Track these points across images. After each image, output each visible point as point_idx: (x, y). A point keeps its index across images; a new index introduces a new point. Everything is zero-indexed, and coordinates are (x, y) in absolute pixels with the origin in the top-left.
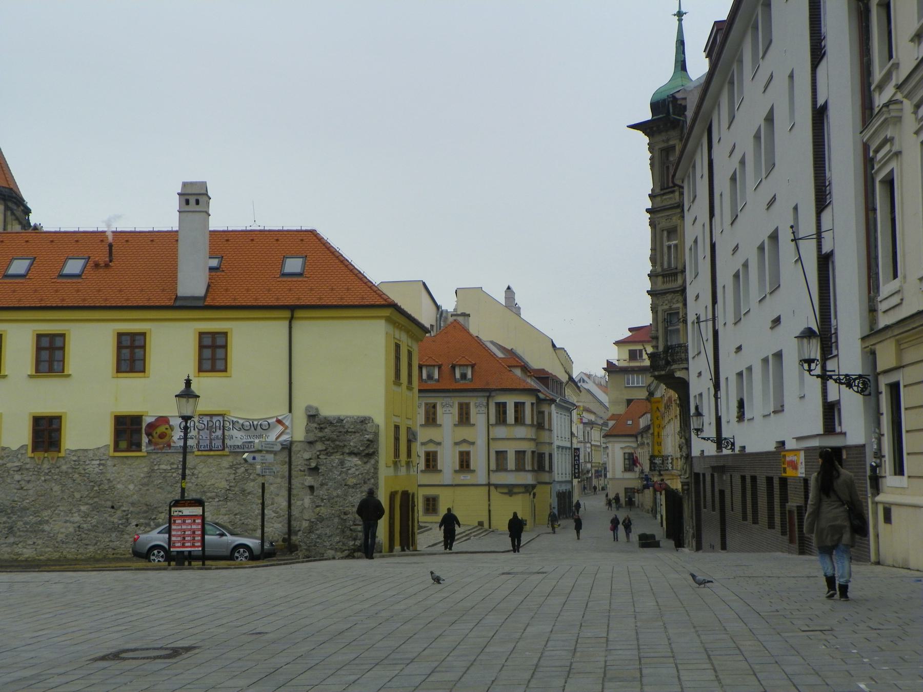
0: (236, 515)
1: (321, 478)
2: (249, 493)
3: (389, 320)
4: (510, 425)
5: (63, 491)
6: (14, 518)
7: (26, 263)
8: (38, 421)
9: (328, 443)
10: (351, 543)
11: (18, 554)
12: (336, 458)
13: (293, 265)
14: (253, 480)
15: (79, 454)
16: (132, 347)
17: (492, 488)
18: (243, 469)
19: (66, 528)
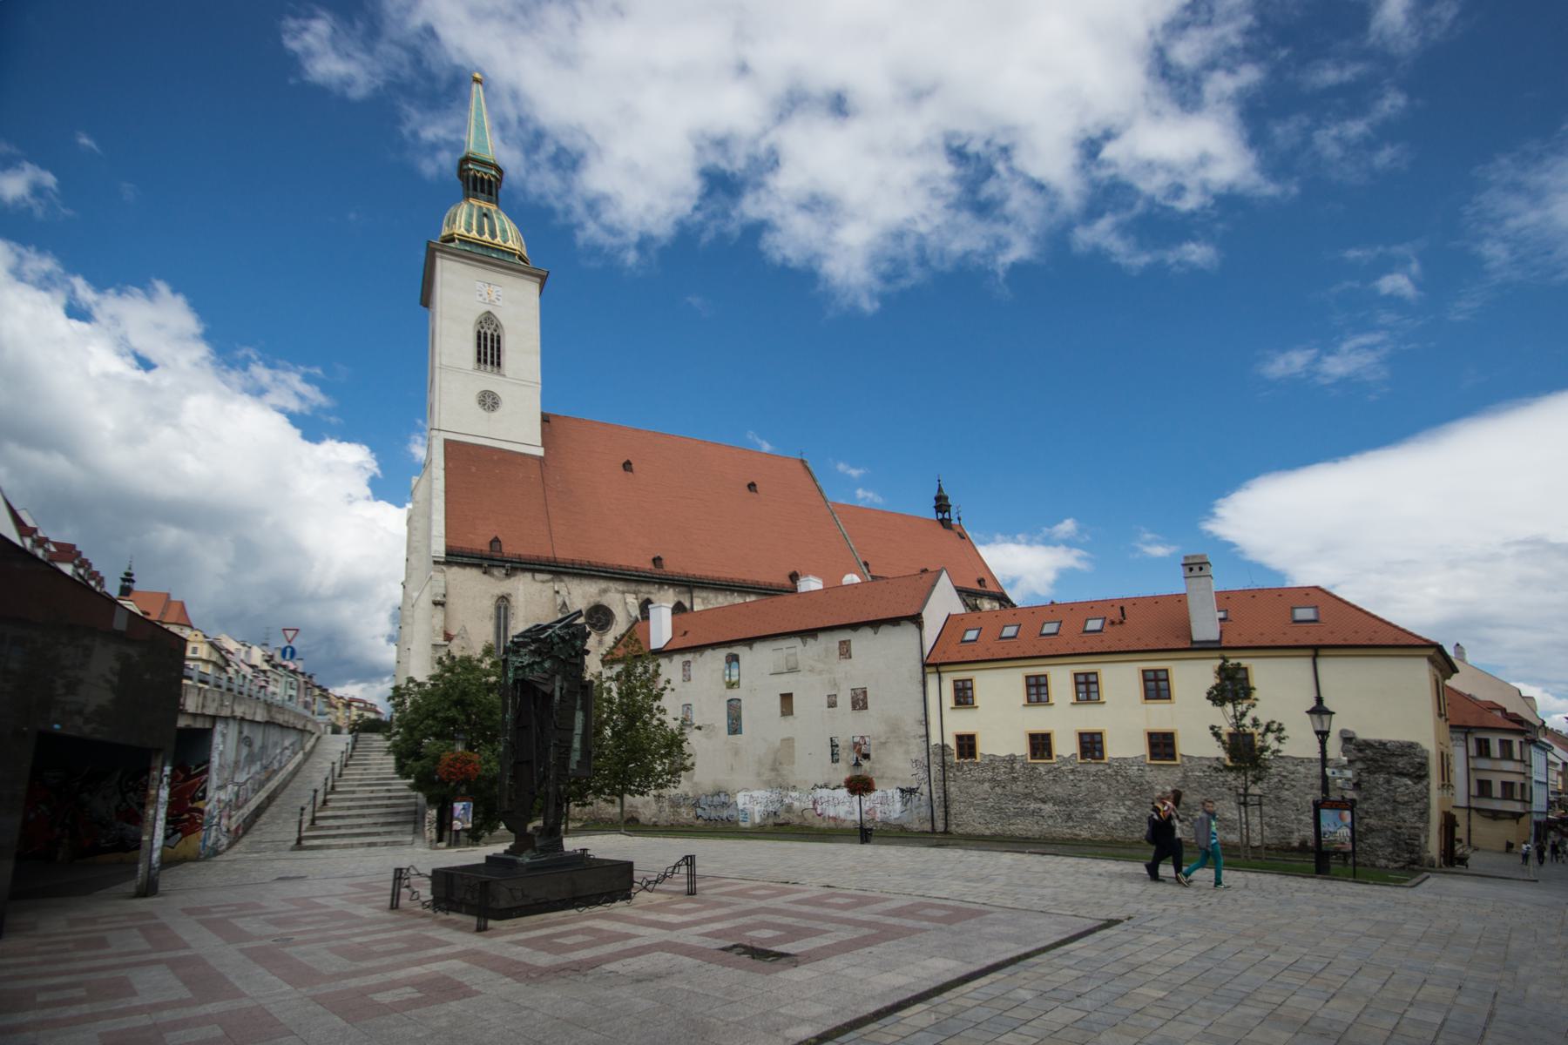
0: (1272, 817)
1: (1365, 793)
2: (1285, 801)
3: (1431, 660)
4: (1496, 759)
5: (1109, 789)
6: (1072, 807)
7: (976, 632)
8: (1152, 736)
9: (1370, 763)
10: (1407, 856)
11: (1076, 835)
12: (1381, 778)
13: (1304, 614)
14: (1287, 790)
15: (1119, 761)
16: (1087, 683)
17: (1473, 813)
18: (1276, 780)
19: (1115, 817)
